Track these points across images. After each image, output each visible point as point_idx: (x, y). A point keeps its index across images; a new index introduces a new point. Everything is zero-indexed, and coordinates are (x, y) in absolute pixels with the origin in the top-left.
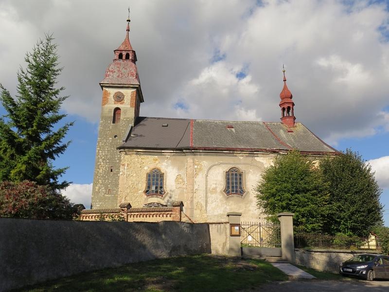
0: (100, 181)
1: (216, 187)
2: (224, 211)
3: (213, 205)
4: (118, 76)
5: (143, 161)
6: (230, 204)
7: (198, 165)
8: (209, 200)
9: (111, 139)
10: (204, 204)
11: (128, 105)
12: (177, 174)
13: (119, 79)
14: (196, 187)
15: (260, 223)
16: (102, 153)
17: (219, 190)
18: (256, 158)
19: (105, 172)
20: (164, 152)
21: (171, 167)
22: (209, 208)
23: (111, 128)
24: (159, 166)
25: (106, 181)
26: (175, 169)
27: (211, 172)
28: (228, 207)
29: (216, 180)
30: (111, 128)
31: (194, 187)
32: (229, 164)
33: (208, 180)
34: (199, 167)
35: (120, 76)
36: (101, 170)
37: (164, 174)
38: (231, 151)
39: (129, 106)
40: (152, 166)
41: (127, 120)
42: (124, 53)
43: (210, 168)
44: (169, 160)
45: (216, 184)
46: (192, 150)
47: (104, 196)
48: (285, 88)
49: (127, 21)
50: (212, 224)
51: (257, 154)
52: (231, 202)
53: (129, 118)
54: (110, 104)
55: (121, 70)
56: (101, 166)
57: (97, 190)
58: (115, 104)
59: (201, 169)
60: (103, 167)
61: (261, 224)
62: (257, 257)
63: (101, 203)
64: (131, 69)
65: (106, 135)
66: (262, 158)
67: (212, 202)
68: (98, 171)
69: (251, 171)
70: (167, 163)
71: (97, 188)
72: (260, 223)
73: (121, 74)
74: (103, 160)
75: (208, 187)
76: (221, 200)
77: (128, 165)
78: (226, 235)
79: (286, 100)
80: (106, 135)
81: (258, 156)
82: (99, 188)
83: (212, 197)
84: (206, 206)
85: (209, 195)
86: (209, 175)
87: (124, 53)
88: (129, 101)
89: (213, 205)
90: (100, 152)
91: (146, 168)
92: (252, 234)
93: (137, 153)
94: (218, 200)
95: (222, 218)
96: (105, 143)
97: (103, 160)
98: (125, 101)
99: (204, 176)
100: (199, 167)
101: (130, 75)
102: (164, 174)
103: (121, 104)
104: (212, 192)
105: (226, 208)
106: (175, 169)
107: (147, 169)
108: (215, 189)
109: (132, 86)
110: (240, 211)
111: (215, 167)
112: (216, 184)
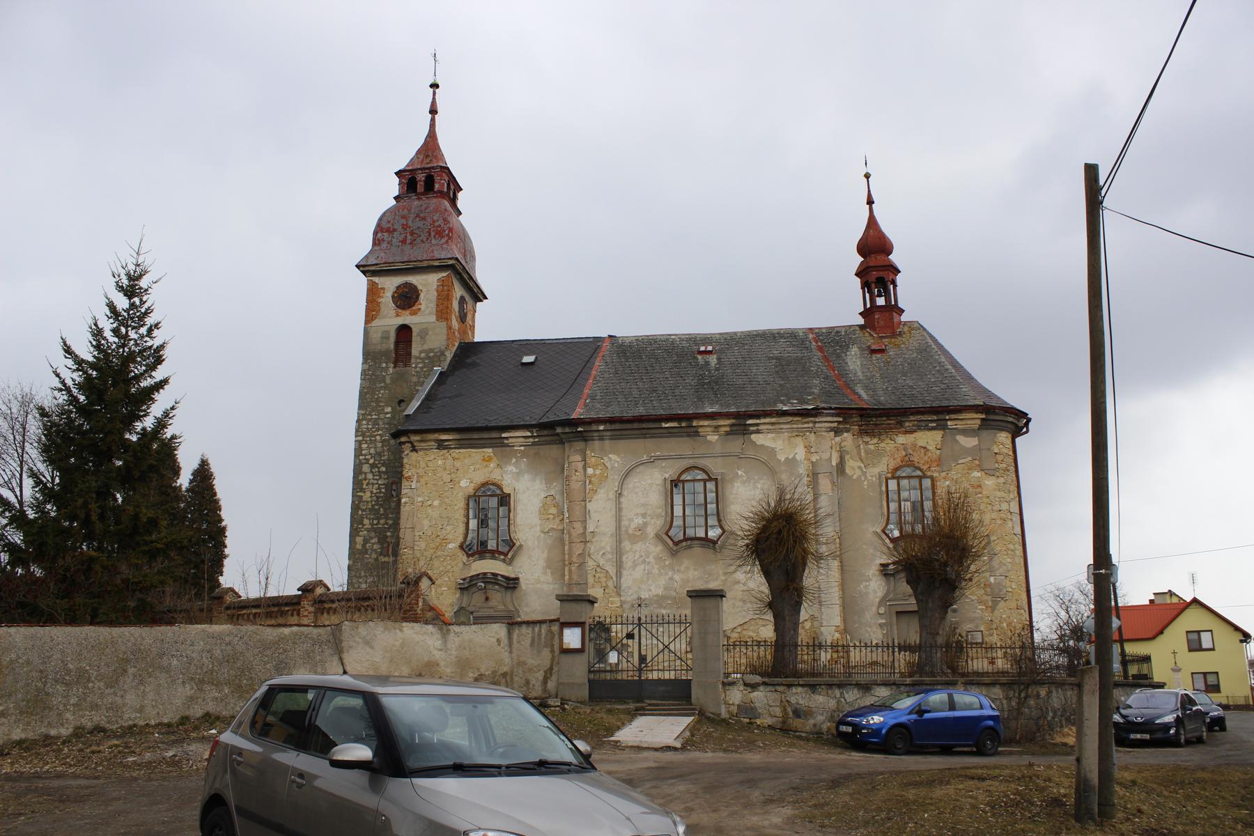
0: (366, 521)
1: (645, 524)
2: (666, 589)
3: (639, 572)
4: (404, 242)
5: (458, 464)
6: (682, 568)
7: (595, 467)
8: (628, 559)
9: (389, 409)
10: (612, 571)
11: (430, 314)
12: (543, 495)
13: (407, 248)
14: (590, 528)
15: (639, 619)
16: (369, 448)
17: (651, 531)
18: (753, 437)
19: (378, 497)
20: (507, 438)
21: (527, 477)
22: (626, 581)
23: (388, 381)
24: (496, 476)
25: (382, 521)
26: (538, 482)
27: (633, 482)
28: (677, 577)
29: (644, 505)
30: (388, 381)
31: (585, 528)
32: (681, 457)
33: (624, 506)
34: (598, 472)
35: (408, 241)
36: (368, 494)
37: (509, 495)
38: (686, 424)
39: (433, 318)
40: (480, 478)
41: (429, 358)
42: (421, 177)
43: (627, 474)
44: (522, 457)
45: (644, 515)
46: (842, 570)
47: (376, 559)
48: (872, 222)
49: (432, 86)
50: (1202, 631)
51: (757, 425)
52: (686, 563)
53: (431, 350)
54: (384, 317)
55: (410, 223)
56: (367, 484)
57: (359, 547)
58: (398, 315)
59: (603, 478)
60: (373, 484)
61: (643, 620)
62: (779, 688)
63: (370, 580)
64: (435, 218)
65: (378, 401)
66: (770, 435)
67: (635, 566)
68: (361, 497)
69: (740, 473)
70: (516, 465)
71: (359, 540)
72: (639, 619)
73: (412, 233)
74: (373, 466)
75: (625, 523)
76: (658, 559)
77: (419, 477)
78: (552, 651)
79: (873, 261)
80: (378, 401)
81: (758, 432)
82: (366, 541)
83: (633, 551)
84: (619, 574)
85: (626, 545)
86: (625, 493)
87: (421, 177)
88: (433, 306)
89: (639, 572)
90: (364, 446)
91: (463, 483)
92: (661, 647)
93: (441, 445)
94: (651, 559)
95: (661, 606)
96: (375, 422)
97: (373, 466)
98: (423, 307)
99: (612, 495)
100: (598, 472)
101: (433, 234)
102: (509, 495)
103: (411, 314)
104: (634, 539)
105: (671, 579)
106: (538, 482)
107: (466, 485)
108: (641, 529)
109: (436, 263)
110: (713, 585)
111: (641, 468)
112: (644, 515)
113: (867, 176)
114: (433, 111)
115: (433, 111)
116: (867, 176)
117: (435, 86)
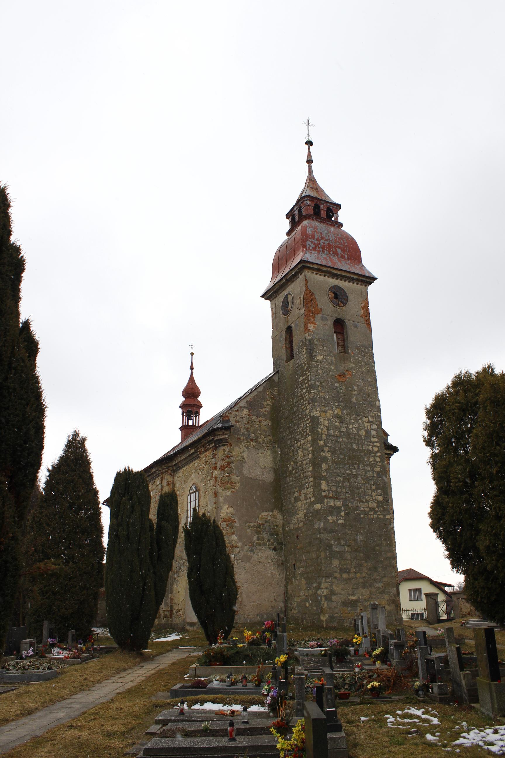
113: (192, 354)
114: (310, 161)
115: (310, 161)
116: (192, 354)
117: (309, 143)
